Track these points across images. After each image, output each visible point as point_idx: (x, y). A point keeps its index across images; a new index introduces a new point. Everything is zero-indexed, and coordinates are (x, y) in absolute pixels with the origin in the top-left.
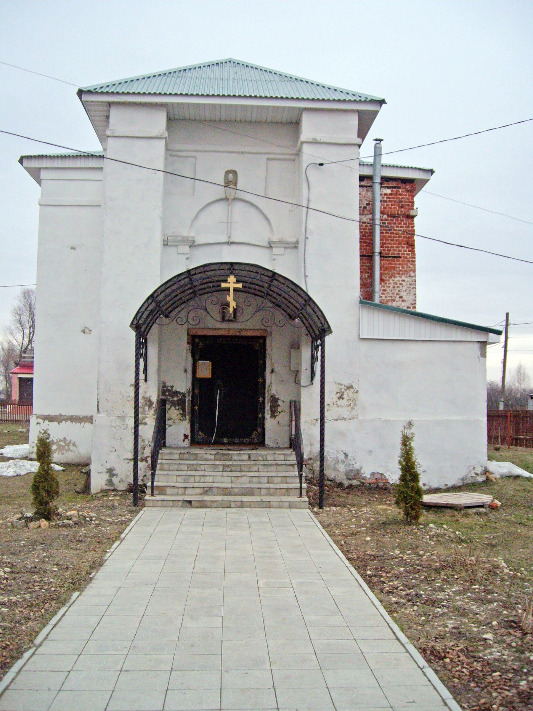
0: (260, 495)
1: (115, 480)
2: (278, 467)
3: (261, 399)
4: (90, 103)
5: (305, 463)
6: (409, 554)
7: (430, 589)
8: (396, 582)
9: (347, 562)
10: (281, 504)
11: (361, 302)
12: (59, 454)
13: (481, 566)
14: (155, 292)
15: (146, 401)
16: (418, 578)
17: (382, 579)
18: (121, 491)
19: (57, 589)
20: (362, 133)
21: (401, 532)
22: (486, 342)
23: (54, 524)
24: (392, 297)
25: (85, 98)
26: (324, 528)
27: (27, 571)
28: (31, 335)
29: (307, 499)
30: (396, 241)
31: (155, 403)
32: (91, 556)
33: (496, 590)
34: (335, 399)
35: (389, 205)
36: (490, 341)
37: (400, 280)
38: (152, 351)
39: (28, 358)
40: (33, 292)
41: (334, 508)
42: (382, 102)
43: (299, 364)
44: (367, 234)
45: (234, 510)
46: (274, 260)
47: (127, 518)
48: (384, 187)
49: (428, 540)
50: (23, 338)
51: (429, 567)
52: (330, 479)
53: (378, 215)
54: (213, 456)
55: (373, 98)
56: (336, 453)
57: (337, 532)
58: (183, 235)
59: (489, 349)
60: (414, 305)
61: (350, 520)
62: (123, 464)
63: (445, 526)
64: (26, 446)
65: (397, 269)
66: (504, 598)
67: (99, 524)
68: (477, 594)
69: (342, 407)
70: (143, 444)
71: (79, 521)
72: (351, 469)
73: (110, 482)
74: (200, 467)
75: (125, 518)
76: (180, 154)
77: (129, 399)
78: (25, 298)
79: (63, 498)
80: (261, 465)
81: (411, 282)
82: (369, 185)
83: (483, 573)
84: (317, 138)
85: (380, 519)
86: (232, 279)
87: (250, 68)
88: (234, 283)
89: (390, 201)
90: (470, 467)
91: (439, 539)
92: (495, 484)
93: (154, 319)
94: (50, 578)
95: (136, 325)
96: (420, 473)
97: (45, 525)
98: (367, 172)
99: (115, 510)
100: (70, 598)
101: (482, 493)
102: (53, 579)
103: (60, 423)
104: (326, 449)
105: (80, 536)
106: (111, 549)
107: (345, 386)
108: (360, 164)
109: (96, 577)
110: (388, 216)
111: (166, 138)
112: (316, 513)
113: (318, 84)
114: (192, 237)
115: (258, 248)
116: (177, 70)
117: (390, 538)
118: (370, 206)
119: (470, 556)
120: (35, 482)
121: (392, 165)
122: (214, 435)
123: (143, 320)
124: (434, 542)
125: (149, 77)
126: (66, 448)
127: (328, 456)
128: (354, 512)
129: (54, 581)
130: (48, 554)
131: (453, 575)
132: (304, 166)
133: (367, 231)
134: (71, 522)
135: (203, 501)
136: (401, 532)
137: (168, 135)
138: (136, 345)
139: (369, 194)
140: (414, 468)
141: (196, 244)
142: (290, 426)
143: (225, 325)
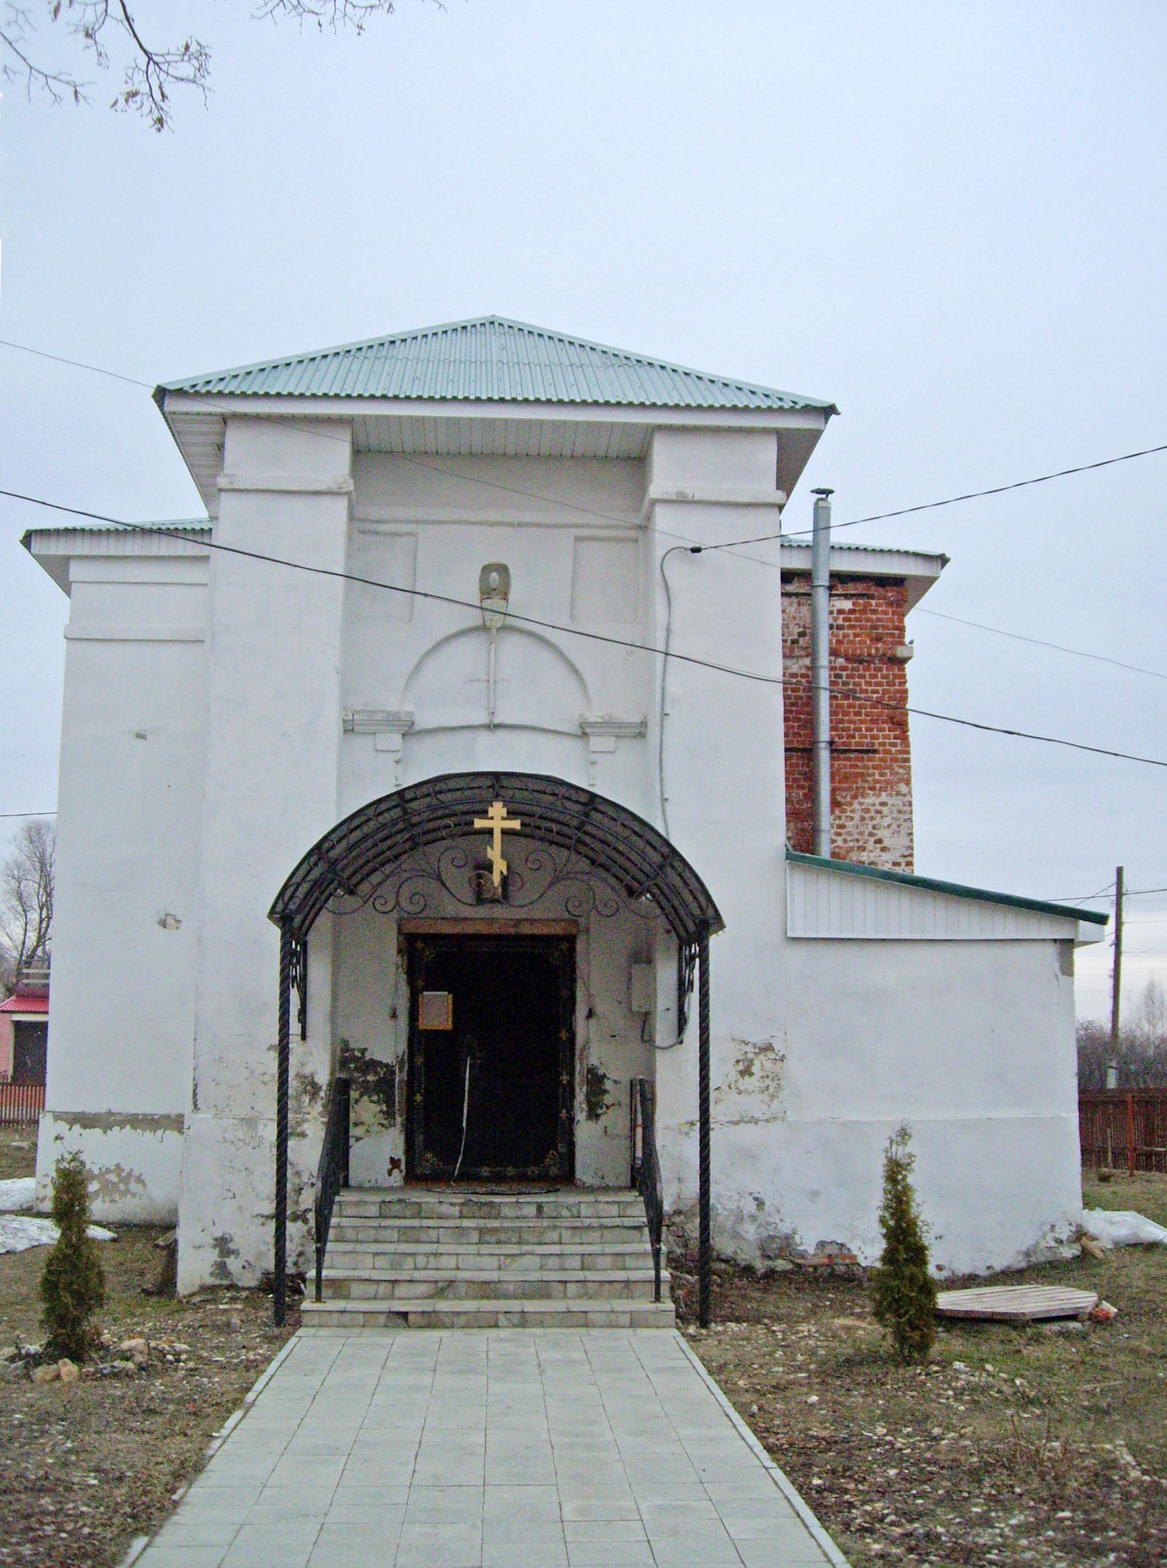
0: (565, 1297)
1: (233, 1264)
2: (605, 1232)
3: (565, 1078)
4: (180, 417)
5: (667, 1222)
6: (908, 1435)
7: (958, 1520)
8: (879, 1505)
9: (764, 1455)
10: (613, 1317)
11: (789, 857)
12: (104, 1201)
13: (1076, 1462)
14: (325, 839)
15: (304, 1083)
16: (930, 1495)
17: (847, 1497)
18: (244, 1289)
19: (97, 1531)
20: (787, 479)
21: (889, 1382)
22: (1072, 940)
23: (92, 1369)
24: (858, 841)
25: (172, 405)
26: (710, 1373)
27: (26, 1487)
28: (44, 925)
29: (672, 1306)
30: (867, 715)
31: (324, 1088)
32: (175, 1447)
33: (1113, 1521)
34: (733, 1075)
35: (848, 636)
36: (1081, 938)
37: (877, 802)
38: (319, 972)
39: (35, 976)
40: (47, 825)
41: (733, 1325)
42: (829, 411)
43: (651, 996)
44: (800, 702)
45: (504, 1333)
46: (593, 763)
47: (260, 1354)
48: (836, 595)
49: (951, 1400)
50: (26, 930)
51: (955, 1465)
52: (723, 1257)
53: (824, 659)
54: (457, 1208)
55: (808, 402)
56: (737, 1197)
57: (741, 1383)
58: (389, 709)
59: (1079, 955)
60: (908, 859)
61: (771, 1354)
62: (252, 1228)
63: (989, 1367)
64: (28, 1183)
65: (870, 779)
66: (1132, 1543)
67: (196, 1369)
68: (1068, 1532)
69: (750, 1093)
70: (297, 1180)
71: (150, 1362)
72: (771, 1234)
73: (221, 1268)
74: (427, 1234)
75: (255, 1355)
76: (382, 528)
77: (266, 1078)
78: (32, 842)
79: (113, 1305)
80: (567, 1228)
81: (901, 807)
82: (802, 591)
83: (1081, 1480)
84: (686, 491)
85: (839, 1350)
86: (497, 810)
87: (537, 337)
88: (503, 819)
89: (851, 627)
90: (1043, 1224)
91: (976, 1398)
92: (1101, 1263)
93: (323, 898)
94: (79, 1503)
95: (282, 915)
96: (930, 1244)
97: (70, 1373)
98: (798, 562)
99: (233, 1335)
100: (126, 1553)
101: (1072, 1286)
102: (89, 1506)
103: (109, 1132)
104: (714, 1190)
105: (152, 1398)
106: (222, 1431)
107: (755, 1046)
108: (782, 546)
109: (186, 1499)
110: (847, 659)
111: (348, 494)
112: (692, 1338)
113: (687, 371)
114: (407, 713)
115: (553, 739)
116: (375, 343)
117: (865, 1396)
118: (807, 638)
119: (1049, 1440)
120: (50, 1272)
121: (853, 547)
122: (460, 1160)
123: (297, 901)
124: (964, 1405)
125: (313, 359)
126: (122, 1187)
127: (719, 1206)
128: (780, 1336)
129: (90, 1510)
130: (75, 1444)
131: (1012, 1486)
132: (659, 553)
133: (801, 693)
134: (130, 1365)
135: (434, 1312)
136: (889, 1382)
137: (355, 487)
138: (282, 960)
139: (804, 610)
140: (915, 1234)
141: (418, 727)
142: (632, 1137)
143: (482, 911)
